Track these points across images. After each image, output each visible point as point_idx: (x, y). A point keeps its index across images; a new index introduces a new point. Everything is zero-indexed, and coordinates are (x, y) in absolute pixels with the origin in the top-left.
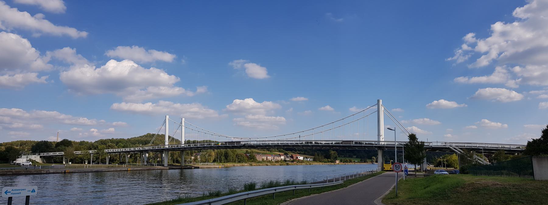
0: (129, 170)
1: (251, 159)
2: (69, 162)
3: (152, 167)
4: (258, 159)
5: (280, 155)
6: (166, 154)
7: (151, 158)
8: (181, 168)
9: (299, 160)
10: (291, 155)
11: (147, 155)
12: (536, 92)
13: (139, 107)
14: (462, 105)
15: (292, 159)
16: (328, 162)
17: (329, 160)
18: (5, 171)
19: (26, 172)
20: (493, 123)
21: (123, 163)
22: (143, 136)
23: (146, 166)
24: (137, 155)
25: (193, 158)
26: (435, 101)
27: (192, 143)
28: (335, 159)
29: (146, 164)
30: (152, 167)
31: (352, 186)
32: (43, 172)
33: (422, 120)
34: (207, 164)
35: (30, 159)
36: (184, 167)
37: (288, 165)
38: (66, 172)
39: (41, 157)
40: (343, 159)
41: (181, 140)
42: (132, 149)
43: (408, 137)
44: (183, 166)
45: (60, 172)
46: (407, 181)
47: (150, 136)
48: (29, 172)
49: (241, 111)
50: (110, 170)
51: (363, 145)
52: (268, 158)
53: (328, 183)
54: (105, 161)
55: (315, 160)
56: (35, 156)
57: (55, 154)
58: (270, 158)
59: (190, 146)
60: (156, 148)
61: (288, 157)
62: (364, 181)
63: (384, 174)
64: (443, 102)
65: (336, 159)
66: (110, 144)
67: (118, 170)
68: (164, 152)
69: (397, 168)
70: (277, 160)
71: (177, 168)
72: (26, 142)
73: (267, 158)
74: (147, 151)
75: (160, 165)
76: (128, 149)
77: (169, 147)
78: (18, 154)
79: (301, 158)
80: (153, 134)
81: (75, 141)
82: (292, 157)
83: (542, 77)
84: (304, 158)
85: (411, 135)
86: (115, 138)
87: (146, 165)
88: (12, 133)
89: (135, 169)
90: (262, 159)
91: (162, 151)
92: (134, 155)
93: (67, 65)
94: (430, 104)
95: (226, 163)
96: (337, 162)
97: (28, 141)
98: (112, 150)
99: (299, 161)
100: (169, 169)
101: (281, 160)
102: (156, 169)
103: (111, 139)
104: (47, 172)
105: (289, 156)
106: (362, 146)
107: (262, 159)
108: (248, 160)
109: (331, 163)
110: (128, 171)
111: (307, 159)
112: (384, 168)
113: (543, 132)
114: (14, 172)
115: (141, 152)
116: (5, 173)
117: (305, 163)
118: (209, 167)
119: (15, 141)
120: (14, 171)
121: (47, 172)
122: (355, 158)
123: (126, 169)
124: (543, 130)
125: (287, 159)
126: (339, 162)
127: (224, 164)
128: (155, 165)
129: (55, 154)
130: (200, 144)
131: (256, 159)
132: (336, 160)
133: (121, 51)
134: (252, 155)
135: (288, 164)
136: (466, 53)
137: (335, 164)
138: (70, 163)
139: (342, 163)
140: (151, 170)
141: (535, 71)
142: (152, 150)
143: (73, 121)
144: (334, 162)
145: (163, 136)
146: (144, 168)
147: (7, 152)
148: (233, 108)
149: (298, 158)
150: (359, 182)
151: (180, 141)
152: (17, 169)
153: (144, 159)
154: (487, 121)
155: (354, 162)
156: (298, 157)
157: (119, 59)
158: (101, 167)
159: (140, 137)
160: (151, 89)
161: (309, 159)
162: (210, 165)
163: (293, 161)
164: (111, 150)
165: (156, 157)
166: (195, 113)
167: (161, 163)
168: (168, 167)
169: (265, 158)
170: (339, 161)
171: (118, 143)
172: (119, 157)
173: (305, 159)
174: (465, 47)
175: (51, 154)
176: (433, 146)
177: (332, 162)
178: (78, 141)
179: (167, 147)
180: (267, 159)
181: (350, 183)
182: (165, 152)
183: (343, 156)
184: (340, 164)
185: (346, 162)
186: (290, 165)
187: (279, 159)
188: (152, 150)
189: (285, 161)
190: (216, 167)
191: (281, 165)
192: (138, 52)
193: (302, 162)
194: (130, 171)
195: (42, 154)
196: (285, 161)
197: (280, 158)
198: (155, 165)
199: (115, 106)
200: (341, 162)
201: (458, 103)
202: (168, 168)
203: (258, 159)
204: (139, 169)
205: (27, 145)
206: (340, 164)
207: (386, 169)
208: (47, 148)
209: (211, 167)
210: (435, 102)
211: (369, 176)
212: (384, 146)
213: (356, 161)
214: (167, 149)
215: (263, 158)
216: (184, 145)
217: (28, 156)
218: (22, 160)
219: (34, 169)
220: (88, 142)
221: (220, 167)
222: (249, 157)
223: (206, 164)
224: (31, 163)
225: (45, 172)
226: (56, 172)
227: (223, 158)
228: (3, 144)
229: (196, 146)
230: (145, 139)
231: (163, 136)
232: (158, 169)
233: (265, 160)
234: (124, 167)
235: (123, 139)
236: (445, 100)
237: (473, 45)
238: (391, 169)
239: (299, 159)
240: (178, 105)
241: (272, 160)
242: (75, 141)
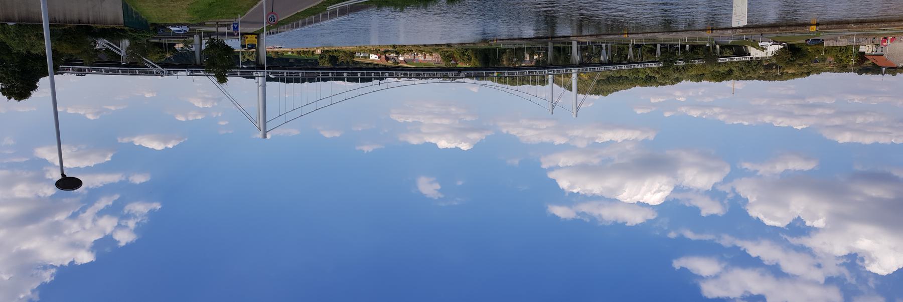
0: (626, 34)
1: (447, 51)
2: (709, 47)
3: (594, 39)
4: (438, 56)
5: (405, 61)
6: (575, 60)
7: (596, 54)
8: (553, 39)
9: (377, 54)
10: (388, 62)
11: (602, 58)
12: (16, 160)
13: (618, 136)
14: (126, 140)
15: (387, 55)
16: (332, 52)
17: (331, 54)
18: (788, 31)
19: (762, 30)
20: (82, 113)
21: (637, 47)
22: (613, 91)
23: (602, 40)
24: (619, 59)
25: (536, 57)
26: (171, 147)
27: (538, 76)
28: (322, 56)
29: (604, 45)
30: (594, 39)
31: (314, 3)
32: (741, 30)
33: (190, 119)
34: (514, 45)
35: (763, 51)
36: (548, 40)
37: (394, 45)
38: (710, 31)
39: (749, 54)
40: (310, 56)
41: (554, 84)
42: (624, 67)
43: (227, 80)
44: (549, 41)
45: (718, 31)
46: (235, 14)
47: (603, 92)
48: (758, 30)
49: (461, 130)
50: (652, 34)
51: (288, 71)
52: (423, 58)
53: (348, 4)
54: (663, 50)
55: (352, 54)
56: (757, 56)
57: (723, 60)
58: (420, 57)
59: (539, 72)
60: (589, 68)
61: (393, 58)
62: (294, 13)
63: (260, 27)
64: (157, 146)
65: (321, 57)
66: (657, 76)
67: (641, 34)
68: (578, 63)
69: (273, 17)
70: (410, 54)
71: (559, 39)
72: (775, 79)
73: (425, 58)
74: (602, 64)
75: (582, 43)
76: (631, 67)
77: (571, 70)
78: (778, 55)
79: (373, 57)
80: (599, 95)
81: (710, 82)
82: (387, 59)
83: (9, 183)
84: (369, 57)
85: (224, 82)
86: (654, 87)
87: (602, 43)
88: (790, 92)
89: (617, 36)
90: (432, 55)
91: (581, 64)
92: (623, 59)
93: (714, 194)
94: (182, 141)
95: (486, 47)
96: (319, 51)
97: (772, 81)
98: (653, 65)
99: (376, 52)
100: (570, 36)
101: (403, 55)
102: (587, 37)
103: (659, 86)
104: (736, 31)
105: (391, 60)
106: (289, 69)
107: (432, 55)
108: (454, 53)
109: (329, 49)
110: (628, 34)
111: (365, 55)
112: (256, 38)
113: (36, 87)
114: (777, 29)
115: (610, 63)
116: (788, 28)
117: (366, 49)
118: (512, 41)
119: (790, 80)
120: (777, 32)
121: (736, 31)
122: (291, 59)
123: (630, 36)
124: (36, 90)
125: (394, 55)
126: (317, 50)
127: (489, 47)
128: (589, 42)
129: (723, 60)
130: (525, 75)
131: (441, 55)
132: (320, 55)
133: (635, 218)
134: (447, 62)
135: (394, 47)
136: (128, 216)
137: (322, 49)
138: (708, 45)
139: (312, 50)
140: (595, 35)
141: (21, 190)
142: (588, 66)
143: (708, 112)
144: (324, 52)
145: (579, 91)
146: (605, 37)
147: (792, 59)
148: (475, 136)
149: (377, 57)
150: (301, 10)
151: (555, 83)
152: (775, 33)
153: (607, 53)
154: (90, 117)
155: (292, 52)
156: (379, 58)
157: (643, 205)
158: (664, 37)
159: (617, 91)
160: (596, 161)
161: (362, 55)
162: (510, 45)
163: (386, 51)
164: (654, 65)
165: (589, 57)
166: (530, 128)
167: (583, 48)
168: (572, 40)
169: (428, 57)
170: (317, 53)
171: (649, 80)
172: (644, 56)
173: (367, 56)
174: (132, 224)
175: (735, 59)
176: (186, 70)
177: (327, 51)
178: (704, 82)
179: (573, 71)
180: (425, 55)
181: (316, 9)
182: (576, 62)
183: (309, 61)
184: (315, 49)
185: (305, 52)
186: (391, 46)
187: (407, 56)
188: (596, 66)
189: (397, 53)
190: (501, 41)
191: (404, 45)
192: (608, 214)
193: (371, 52)
194: (625, 32)
195: (748, 58)
196: (397, 53)
197: (406, 58)
198: (589, 42)
199: (651, 136)
200: (313, 52)
201: (132, 144)
202: (571, 38)
203: (438, 56)
204: (612, 36)
205: (774, 75)
206: (315, 49)
207: (254, 36)
208: (743, 68)
209: (509, 42)
210: (170, 146)
211: (284, 23)
212: (257, 69)
213: (289, 53)
214: (573, 67)
215: (431, 57)
216: (549, 73)
217: (765, 56)
218: (772, 49)
219: (752, 34)
220: (691, 81)
221: (495, 41)
222: (451, 59)
223: (516, 45)
224: (760, 44)
225: (738, 30)
226: (724, 31)
227: (491, 56)
228: (805, 75)
229: (530, 71)
230: (610, 87)
231: (579, 91)
232: (584, 37)
233: (428, 54)
234: (633, 39)
235: (641, 86)
236: (153, 149)
237: (119, 226)
238: (247, 36)
239: (376, 56)
240: (559, 140)
241: (417, 55)
242: (710, 82)
